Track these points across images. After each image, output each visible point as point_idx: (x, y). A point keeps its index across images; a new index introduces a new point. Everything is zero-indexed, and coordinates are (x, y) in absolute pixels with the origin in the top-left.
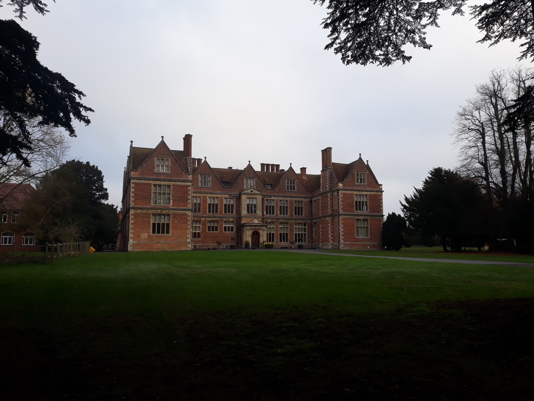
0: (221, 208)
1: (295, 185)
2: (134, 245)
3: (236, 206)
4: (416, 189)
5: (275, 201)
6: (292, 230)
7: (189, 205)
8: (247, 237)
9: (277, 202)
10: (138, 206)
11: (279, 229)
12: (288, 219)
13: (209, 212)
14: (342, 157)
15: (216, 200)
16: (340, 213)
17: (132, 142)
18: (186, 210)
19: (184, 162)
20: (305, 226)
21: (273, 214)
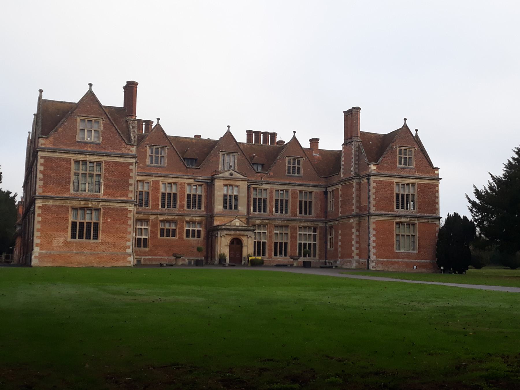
0: (182, 200)
2: (41, 257)
4: (492, 176)
5: (269, 191)
6: (294, 238)
8: (223, 247)
9: (271, 192)
10: (48, 194)
11: (274, 236)
12: (288, 220)
15: (174, 187)
16: (372, 212)
17: (41, 91)
18: (126, 202)
19: (125, 125)
20: (315, 231)
21: (265, 211)
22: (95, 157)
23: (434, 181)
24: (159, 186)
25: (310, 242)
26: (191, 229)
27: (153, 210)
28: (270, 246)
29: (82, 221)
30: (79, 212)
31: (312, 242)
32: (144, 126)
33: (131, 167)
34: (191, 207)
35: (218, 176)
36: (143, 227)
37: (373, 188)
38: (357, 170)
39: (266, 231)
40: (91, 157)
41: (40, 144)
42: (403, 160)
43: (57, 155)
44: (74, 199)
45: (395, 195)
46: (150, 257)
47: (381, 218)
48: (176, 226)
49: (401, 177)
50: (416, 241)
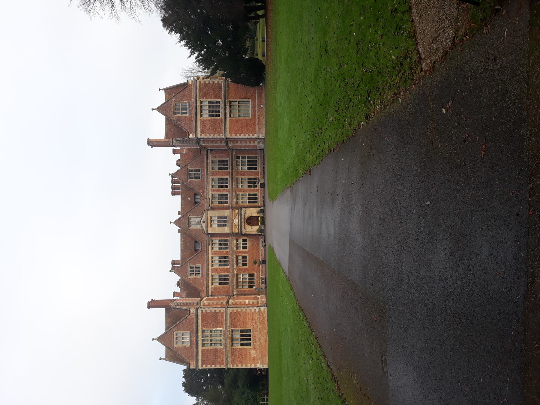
0: (223, 253)
2: (262, 363)
3: (220, 237)
4: (190, 56)
5: (213, 193)
6: (244, 174)
7: (222, 311)
8: (253, 229)
9: (213, 191)
10: (225, 361)
12: (232, 178)
14: (158, 127)
15: (214, 277)
17: (161, 359)
18: (226, 314)
20: (238, 158)
26: (241, 246)
28: (251, 191)
30: (234, 342)
31: (247, 159)
33: (204, 312)
38: (194, 142)
43: (200, 357)
45: (210, 118)
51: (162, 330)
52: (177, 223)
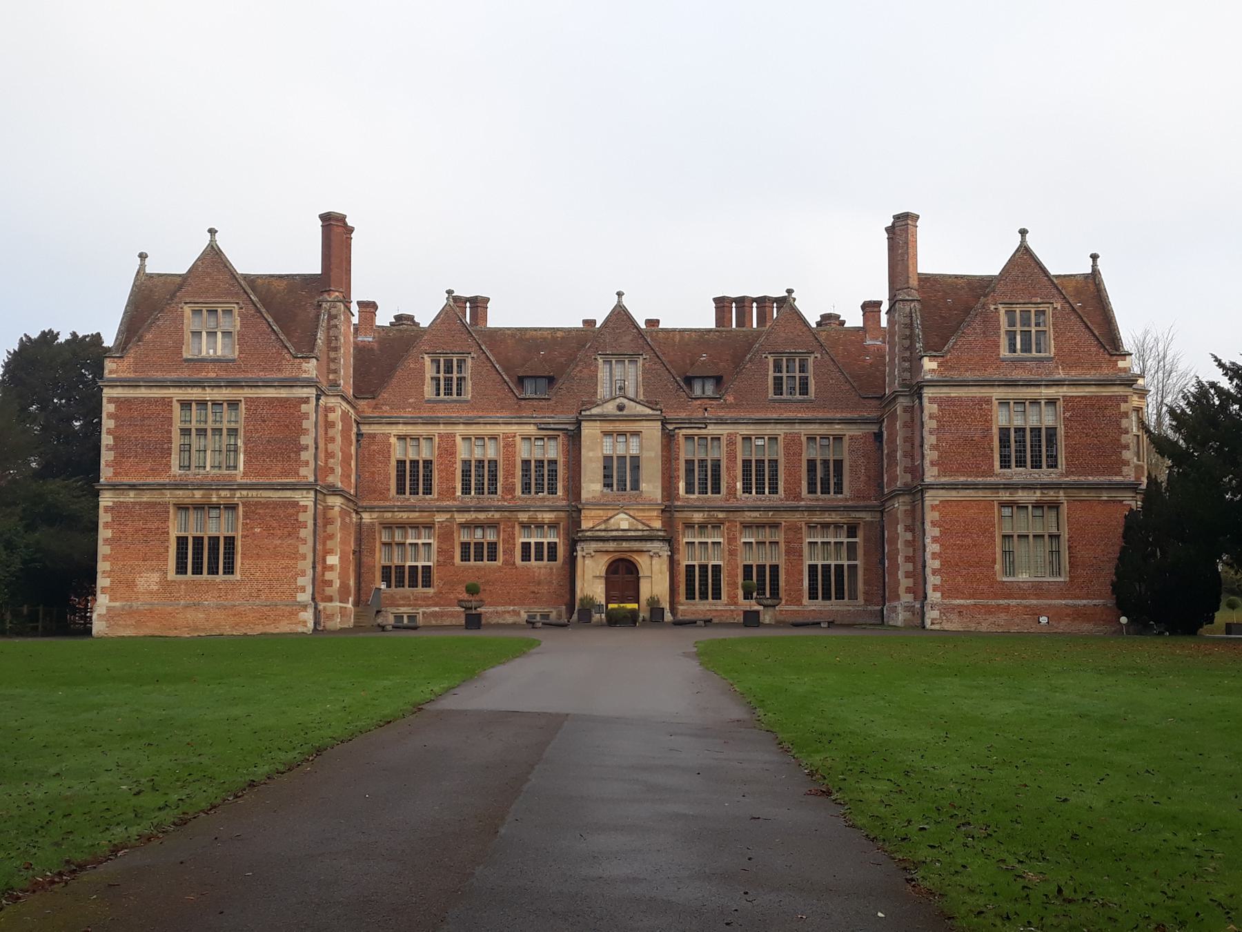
0: (510, 474)
1: (467, 373)
2: (111, 615)
4: (1221, 365)
5: (724, 442)
6: (794, 552)
7: (303, 471)
8: (592, 583)
9: (731, 443)
11: (740, 548)
12: (776, 510)
13: (466, 490)
16: (928, 479)
17: (143, 256)
18: (293, 487)
19: (312, 313)
20: (852, 532)
21: (716, 490)
22: (224, 391)
23: (1115, 389)
24: (455, 444)
25: (839, 562)
27: (443, 500)
28: (732, 576)
29: (199, 534)
32: (755, 310)
33: (304, 407)
34: (533, 490)
35: (588, 413)
36: (420, 542)
37: (930, 418)
38: (907, 375)
39: (721, 540)
40: (216, 391)
41: (106, 372)
42: (1018, 338)
43: (143, 393)
44: (176, 486)
46: (437, 609)
47: (954, 493)
48: (498, 536)
49: (1013, 384)
50: (1062, 550)
51: (249, 259)
52: (620, 315)
